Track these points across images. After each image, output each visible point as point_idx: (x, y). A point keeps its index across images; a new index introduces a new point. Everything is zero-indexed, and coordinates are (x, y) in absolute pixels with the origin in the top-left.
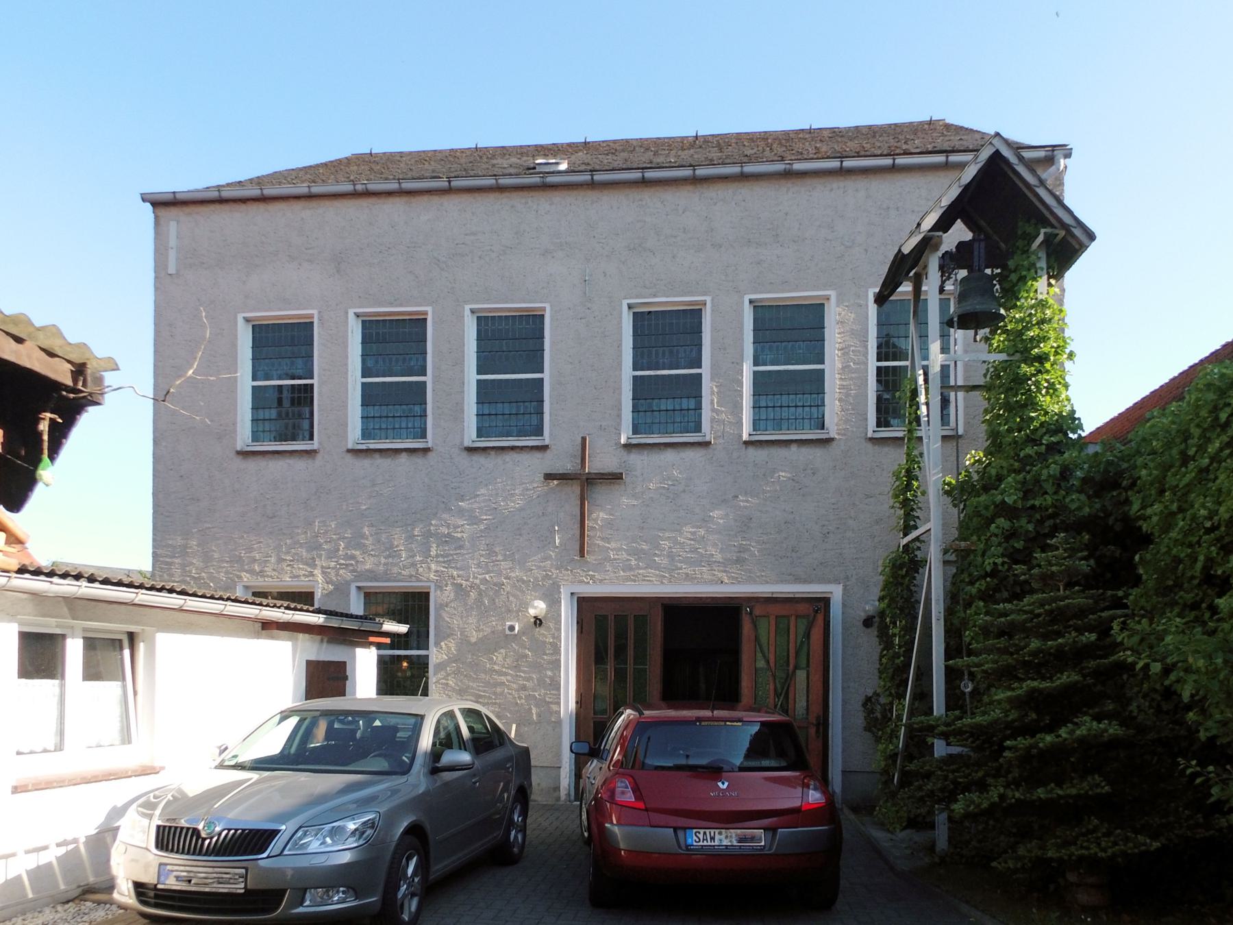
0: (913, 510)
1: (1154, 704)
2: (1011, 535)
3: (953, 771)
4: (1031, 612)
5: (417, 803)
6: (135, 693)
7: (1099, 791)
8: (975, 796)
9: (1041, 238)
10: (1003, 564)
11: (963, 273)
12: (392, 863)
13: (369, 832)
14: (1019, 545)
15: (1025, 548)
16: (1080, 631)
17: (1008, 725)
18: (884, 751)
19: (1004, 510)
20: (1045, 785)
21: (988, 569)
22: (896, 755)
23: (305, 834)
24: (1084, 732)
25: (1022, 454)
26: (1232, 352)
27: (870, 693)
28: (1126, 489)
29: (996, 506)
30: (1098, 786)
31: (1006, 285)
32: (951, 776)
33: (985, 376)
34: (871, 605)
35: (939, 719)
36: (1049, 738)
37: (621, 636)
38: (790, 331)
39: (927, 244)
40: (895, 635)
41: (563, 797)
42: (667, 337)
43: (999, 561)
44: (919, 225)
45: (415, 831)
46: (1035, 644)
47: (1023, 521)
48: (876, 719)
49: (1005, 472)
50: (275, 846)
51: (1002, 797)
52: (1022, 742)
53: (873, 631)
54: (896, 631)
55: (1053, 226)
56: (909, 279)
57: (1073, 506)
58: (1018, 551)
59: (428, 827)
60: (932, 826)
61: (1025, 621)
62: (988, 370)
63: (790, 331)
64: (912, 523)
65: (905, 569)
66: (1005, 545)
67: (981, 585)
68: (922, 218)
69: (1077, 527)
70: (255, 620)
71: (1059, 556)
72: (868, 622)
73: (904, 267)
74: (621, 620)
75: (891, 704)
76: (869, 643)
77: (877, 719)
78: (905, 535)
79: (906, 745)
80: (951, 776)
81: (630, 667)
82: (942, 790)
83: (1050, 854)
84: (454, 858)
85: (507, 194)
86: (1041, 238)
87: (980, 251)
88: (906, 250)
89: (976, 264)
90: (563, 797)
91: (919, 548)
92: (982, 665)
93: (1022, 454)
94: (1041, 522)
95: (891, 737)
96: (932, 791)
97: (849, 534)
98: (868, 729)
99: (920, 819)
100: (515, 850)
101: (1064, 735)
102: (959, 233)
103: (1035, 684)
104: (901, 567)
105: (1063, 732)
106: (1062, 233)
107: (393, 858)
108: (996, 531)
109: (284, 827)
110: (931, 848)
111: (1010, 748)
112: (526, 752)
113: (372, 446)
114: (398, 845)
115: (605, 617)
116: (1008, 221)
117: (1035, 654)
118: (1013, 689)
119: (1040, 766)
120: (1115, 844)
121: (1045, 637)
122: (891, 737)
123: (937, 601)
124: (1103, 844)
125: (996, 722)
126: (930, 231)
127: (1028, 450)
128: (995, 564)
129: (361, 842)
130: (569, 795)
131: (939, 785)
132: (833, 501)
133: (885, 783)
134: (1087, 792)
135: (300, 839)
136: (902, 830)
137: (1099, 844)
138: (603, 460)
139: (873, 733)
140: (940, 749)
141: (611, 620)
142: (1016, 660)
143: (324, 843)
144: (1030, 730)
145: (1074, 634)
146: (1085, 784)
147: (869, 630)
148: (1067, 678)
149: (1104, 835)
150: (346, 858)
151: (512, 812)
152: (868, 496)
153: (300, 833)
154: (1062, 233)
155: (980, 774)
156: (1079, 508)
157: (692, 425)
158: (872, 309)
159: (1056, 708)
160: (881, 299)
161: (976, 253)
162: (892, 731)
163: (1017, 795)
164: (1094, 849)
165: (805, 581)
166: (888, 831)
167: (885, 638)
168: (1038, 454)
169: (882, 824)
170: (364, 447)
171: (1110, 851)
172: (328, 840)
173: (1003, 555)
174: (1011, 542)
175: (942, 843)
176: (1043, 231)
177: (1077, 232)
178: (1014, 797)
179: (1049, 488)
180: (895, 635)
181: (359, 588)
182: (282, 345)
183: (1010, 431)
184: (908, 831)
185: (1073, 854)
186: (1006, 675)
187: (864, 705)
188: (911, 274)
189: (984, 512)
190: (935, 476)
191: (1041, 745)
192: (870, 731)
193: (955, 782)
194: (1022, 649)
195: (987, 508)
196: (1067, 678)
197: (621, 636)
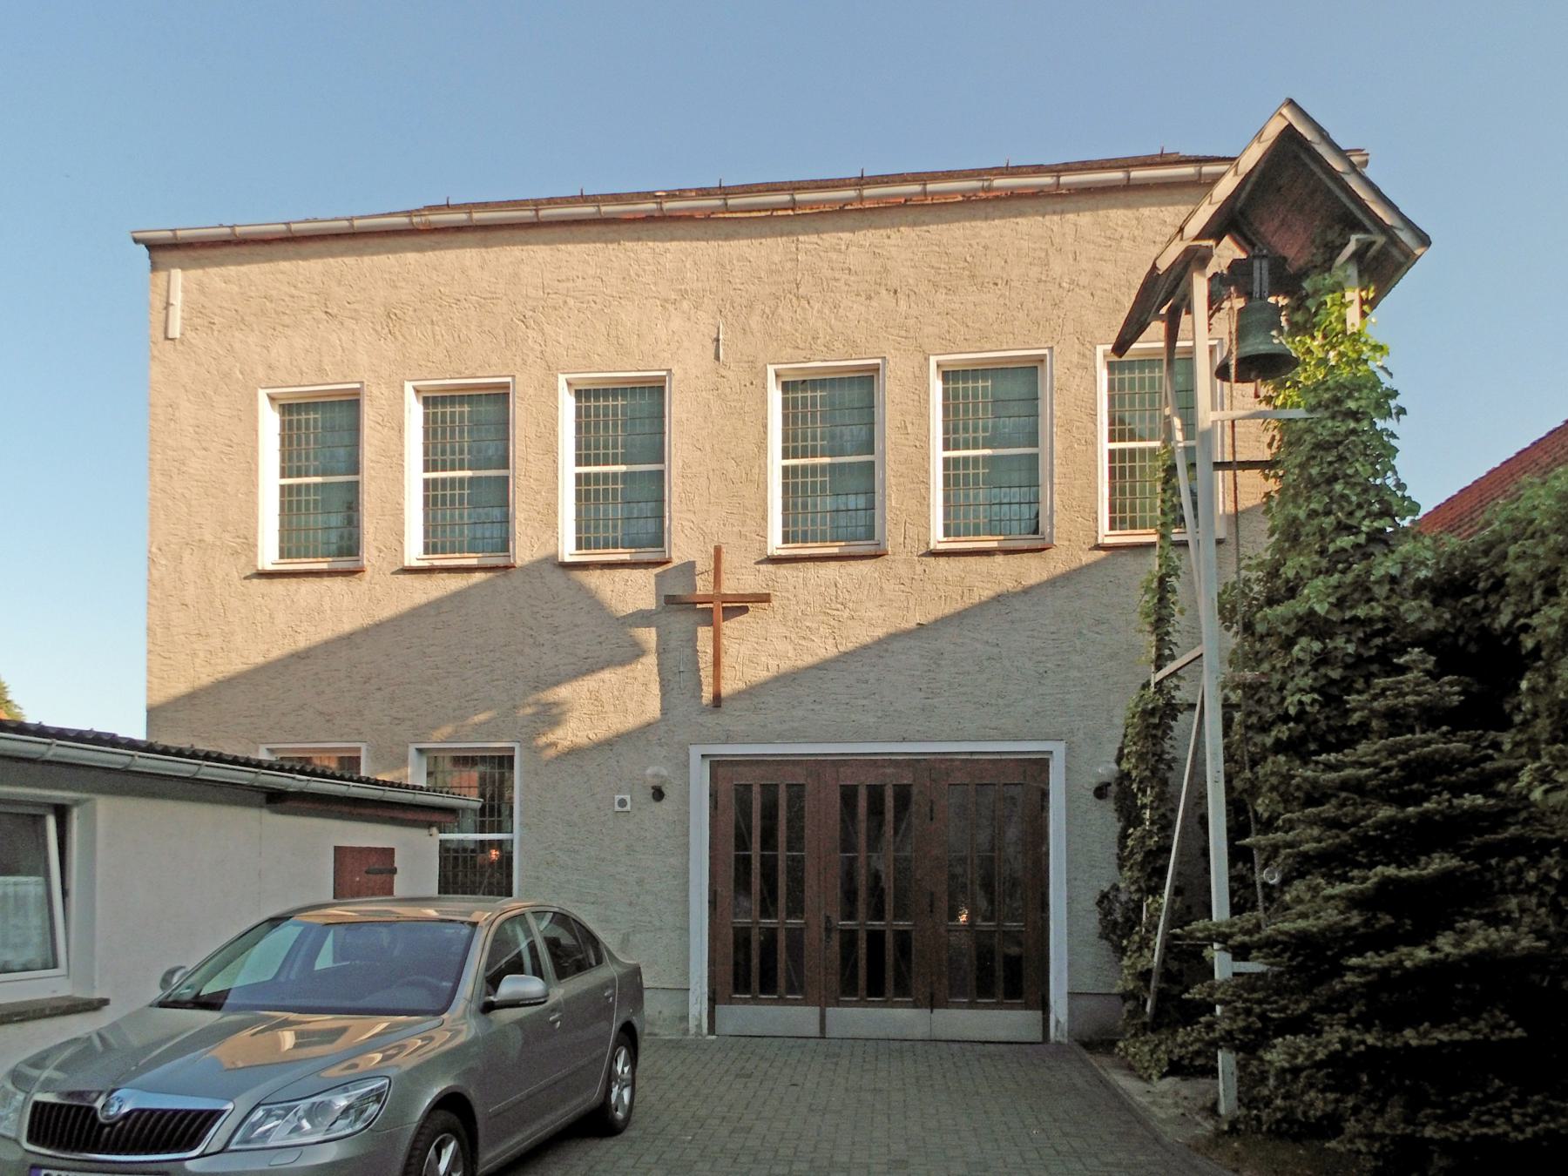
0: (1168, 633)
1: (1547, 900)
2: (1322, 660)
3: (1259, 1002)
4: (1375, 764)
5: (452, 1057)
6: (65, 893)
7: (1506, 1035)
8: (1300, 1040)
9: (1351, 248)
10: (1314, 701)
11: (1239, 303)
12: (410, 1157)
13: (373, 1108)
14: (1335, 674)
15: (1343, 679)
16: (1457, 791)
17: (1350, 931)
18: (1133, 966)
19: (1311, 625)
20: (1415, 1024)
21: (1292, 711)
22: (1149, 971)
23: (268, 1114)
24: (1483, 945)
25: (1332, 548)
26: (1567, 443)
27: (1106, 887)
28: (1486, 593)
29: (1300, 619)
30: (1502, 1027)
31: (1299, 317)
32: (1257, 1009)
33: (1270, 445)
34: (1106, 769)
35: (1219, 925)
36: (1422, 953)
37: (770, 814)
38: (997, 398)
39: (1194, 259)
40: (1144, 806)
41: (693, 1030)
42: (836, 409)
43: (1307, 699)
44: (1181, 230)
45: (454, 1105)
46: (1385, 812)
47: (1340, 641)
48: (1115, 923)
49: (1308, 574)
50: (216, 1136)
51: (1345, 1042)
52: (1372, 959)
53: (1110, 805)
54: (1147, 800)
55: (1367, 231)
56: (1161, 318)
57: (1411, 619)
58: (1332, 682)
59: (472, 1094)
60: (1212, 1072)
61: (1368, 778)
62: (1273, 438)
63: (997, 398)
64: (1167, 652)
65: (1158, 717)
66: (1312, 674)
67: (1282, 732)
68: (1186, 221)
69: (1429, 642)
70: (252, 788)
71: (1417, 680)
72: (1100, 792)
73: (1162, 296)
74: (769, 791)
75: (1141, 901)
76: (1106, 818)
77: (1118, 925)
78: (1159, 668)
79: (1163, 962)
80: (1257, 1009)
81: (782, 854)
82: (1246, 1030)
83: (1429, 1132)
84: (535, 1127)
85: (615, 227)
86: (1351, 248)
87: (1261, 271)
88: (1163, 265)
89: (1256, 289)
90: (693, 1030)
91: (1177, 687)
92: (1300, 843)
93: (1332, 548)
94: (1364, 642)
95: (1140, 949)
96: (1230, 1033)
97: (1075, 673)
98: (1104, 936)
99: (1186, 1062)
100: (620, 1114)
101: (1448, 949)
102: (1227, 252)
103: (1391, 871)
104: (1153, 712)
105: (1445, 943)
106: (1381, 240)
107: (413, 1147)
108: (1301, 655)
109: (230, 1106)
110: (1213, 1110)
111: (1352, 969)
112: (636, 972)
113: (437, 563)
114: (422, 1126)
115: (748, 787)
116: (1304, 224)
117: (1384, 826)
118: (1350, 880)
119: (1394, 999)
120: (1536, 1120)
121: (1401, 801)
122: (1140, 949)
123: (1214, 755)
124: (1517, 1119)
125: (1330, 928)
126: (1197, 238)
127: (1345, 541)
128: (1301, 702)
129: (359, 1126)
130: (699, 1026)
131: (1241, 1024)
132: (1053, 629)
133: (1133, 1014)
134: (1487, 1038)
135: (260, 1123)
136: (1163, 1076)
137: (1509, 1120)
138: (741, 579)
139: (1111, 941)
140: (1223, 965)
141: (756, 790)
142: (1354, 836)
143: (297, 1129)
144: (1383, 941)
145: (1446, 795)
146: (1482, 1024)
147: (1102, 802)
148: (1437, 863)
149: (1515, 1104)
150: (331, 1153)
151: (614, 1060)
152: (1099, 622)
153: (260, 1113)
154: (1381, 240)
155: (1304, 1006)
156: (1421, 620)
157: (862, 529)
158: (1103, 375)
159: (1423, 909)
160: (1121, 347)
161: (1256, 275)
162: (1142, 938)
163: (1370, 1040)
164: (1501, 1127)
165: (1016, 739)
166: (1140, 1077)
167: (1130, 816)
168: (1357, 546)
169: (1131, 1068)
170: (425, 564)
171: (1529, 1131)
172: (306, 1125)
173: (1313, 690)
174: (1322, 670)
175: (1227, 1106)
176: (1354, 238)
177: (1405, 236)
178: (1363, 1042)
179: (1381, 591)
180: (1144, 806)
181: (420, 751)
182: (325, 430)
183: (1313, 514)
184: (1170, 1080)
185: (1466, 1133)
186: (1331, 862)
187: (1099, 903)
188: (1163, 311)
189: (1282, 629)
190: (1202, 585)
191: (1408, 964)
192: (1107, 938)
193: (1263, 1017)
194: (1364, 818)
195: (1287, 623)
196: (1437, 863)
197: (770, 814)
